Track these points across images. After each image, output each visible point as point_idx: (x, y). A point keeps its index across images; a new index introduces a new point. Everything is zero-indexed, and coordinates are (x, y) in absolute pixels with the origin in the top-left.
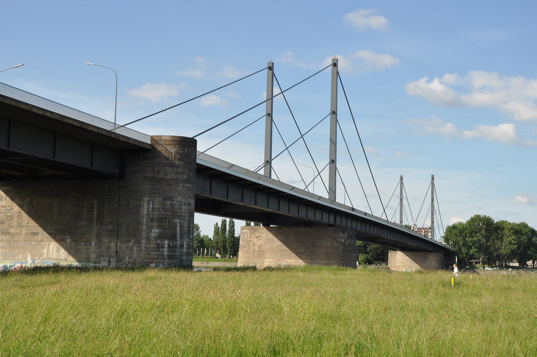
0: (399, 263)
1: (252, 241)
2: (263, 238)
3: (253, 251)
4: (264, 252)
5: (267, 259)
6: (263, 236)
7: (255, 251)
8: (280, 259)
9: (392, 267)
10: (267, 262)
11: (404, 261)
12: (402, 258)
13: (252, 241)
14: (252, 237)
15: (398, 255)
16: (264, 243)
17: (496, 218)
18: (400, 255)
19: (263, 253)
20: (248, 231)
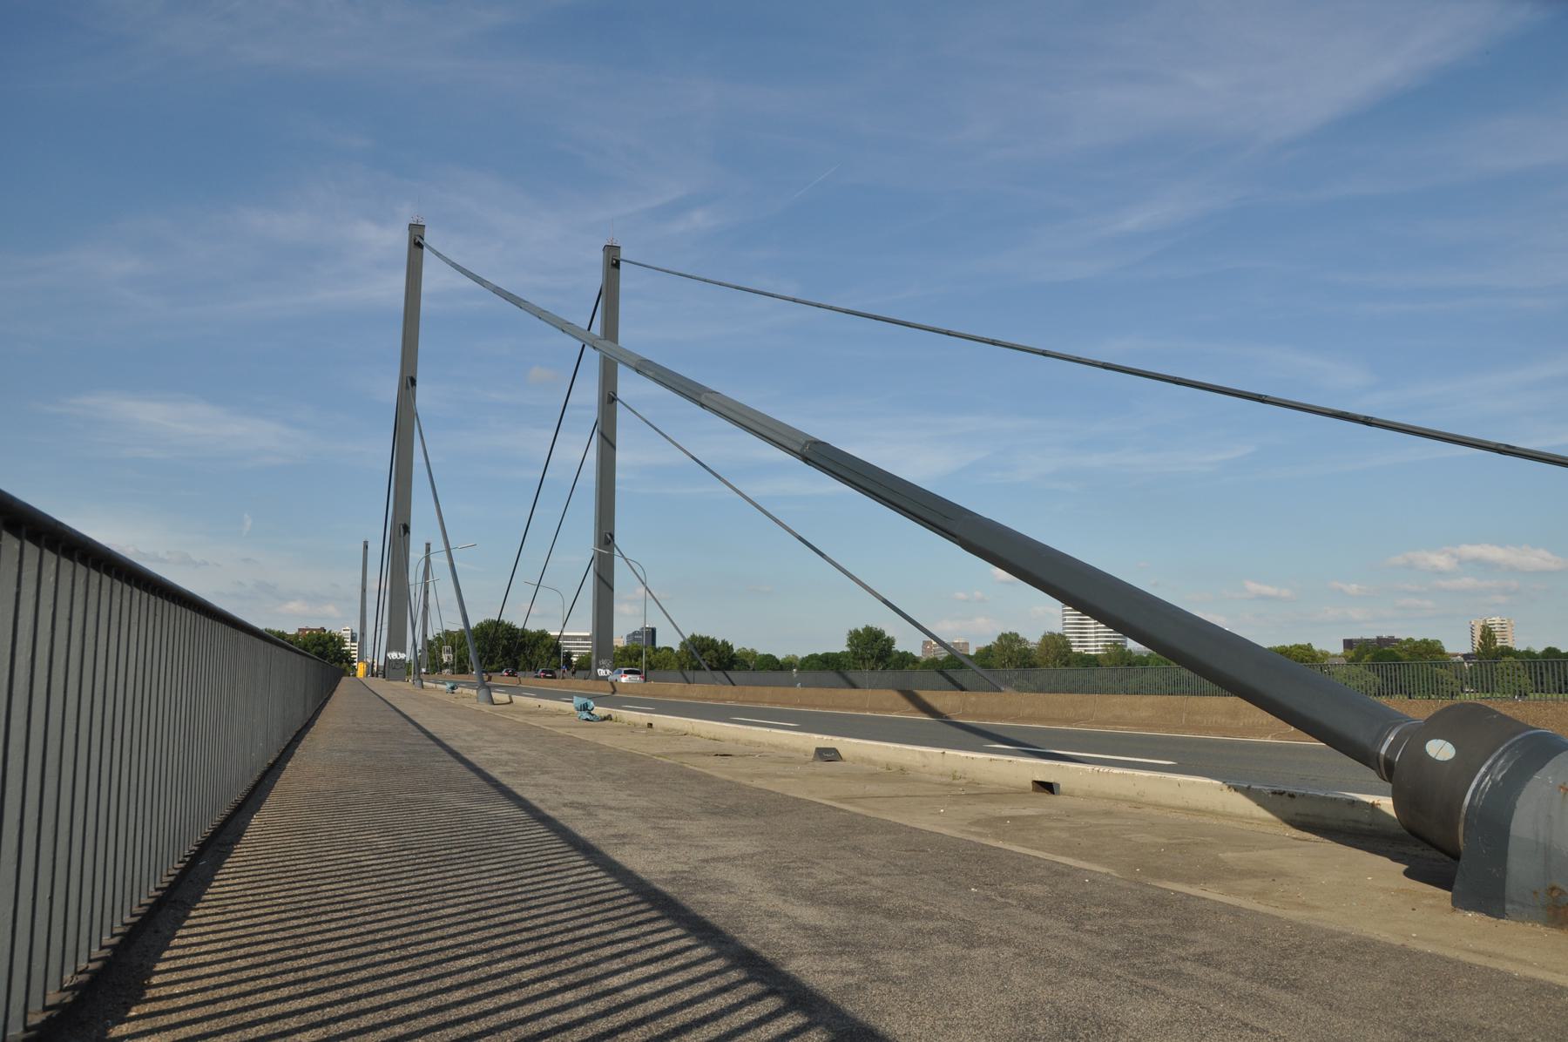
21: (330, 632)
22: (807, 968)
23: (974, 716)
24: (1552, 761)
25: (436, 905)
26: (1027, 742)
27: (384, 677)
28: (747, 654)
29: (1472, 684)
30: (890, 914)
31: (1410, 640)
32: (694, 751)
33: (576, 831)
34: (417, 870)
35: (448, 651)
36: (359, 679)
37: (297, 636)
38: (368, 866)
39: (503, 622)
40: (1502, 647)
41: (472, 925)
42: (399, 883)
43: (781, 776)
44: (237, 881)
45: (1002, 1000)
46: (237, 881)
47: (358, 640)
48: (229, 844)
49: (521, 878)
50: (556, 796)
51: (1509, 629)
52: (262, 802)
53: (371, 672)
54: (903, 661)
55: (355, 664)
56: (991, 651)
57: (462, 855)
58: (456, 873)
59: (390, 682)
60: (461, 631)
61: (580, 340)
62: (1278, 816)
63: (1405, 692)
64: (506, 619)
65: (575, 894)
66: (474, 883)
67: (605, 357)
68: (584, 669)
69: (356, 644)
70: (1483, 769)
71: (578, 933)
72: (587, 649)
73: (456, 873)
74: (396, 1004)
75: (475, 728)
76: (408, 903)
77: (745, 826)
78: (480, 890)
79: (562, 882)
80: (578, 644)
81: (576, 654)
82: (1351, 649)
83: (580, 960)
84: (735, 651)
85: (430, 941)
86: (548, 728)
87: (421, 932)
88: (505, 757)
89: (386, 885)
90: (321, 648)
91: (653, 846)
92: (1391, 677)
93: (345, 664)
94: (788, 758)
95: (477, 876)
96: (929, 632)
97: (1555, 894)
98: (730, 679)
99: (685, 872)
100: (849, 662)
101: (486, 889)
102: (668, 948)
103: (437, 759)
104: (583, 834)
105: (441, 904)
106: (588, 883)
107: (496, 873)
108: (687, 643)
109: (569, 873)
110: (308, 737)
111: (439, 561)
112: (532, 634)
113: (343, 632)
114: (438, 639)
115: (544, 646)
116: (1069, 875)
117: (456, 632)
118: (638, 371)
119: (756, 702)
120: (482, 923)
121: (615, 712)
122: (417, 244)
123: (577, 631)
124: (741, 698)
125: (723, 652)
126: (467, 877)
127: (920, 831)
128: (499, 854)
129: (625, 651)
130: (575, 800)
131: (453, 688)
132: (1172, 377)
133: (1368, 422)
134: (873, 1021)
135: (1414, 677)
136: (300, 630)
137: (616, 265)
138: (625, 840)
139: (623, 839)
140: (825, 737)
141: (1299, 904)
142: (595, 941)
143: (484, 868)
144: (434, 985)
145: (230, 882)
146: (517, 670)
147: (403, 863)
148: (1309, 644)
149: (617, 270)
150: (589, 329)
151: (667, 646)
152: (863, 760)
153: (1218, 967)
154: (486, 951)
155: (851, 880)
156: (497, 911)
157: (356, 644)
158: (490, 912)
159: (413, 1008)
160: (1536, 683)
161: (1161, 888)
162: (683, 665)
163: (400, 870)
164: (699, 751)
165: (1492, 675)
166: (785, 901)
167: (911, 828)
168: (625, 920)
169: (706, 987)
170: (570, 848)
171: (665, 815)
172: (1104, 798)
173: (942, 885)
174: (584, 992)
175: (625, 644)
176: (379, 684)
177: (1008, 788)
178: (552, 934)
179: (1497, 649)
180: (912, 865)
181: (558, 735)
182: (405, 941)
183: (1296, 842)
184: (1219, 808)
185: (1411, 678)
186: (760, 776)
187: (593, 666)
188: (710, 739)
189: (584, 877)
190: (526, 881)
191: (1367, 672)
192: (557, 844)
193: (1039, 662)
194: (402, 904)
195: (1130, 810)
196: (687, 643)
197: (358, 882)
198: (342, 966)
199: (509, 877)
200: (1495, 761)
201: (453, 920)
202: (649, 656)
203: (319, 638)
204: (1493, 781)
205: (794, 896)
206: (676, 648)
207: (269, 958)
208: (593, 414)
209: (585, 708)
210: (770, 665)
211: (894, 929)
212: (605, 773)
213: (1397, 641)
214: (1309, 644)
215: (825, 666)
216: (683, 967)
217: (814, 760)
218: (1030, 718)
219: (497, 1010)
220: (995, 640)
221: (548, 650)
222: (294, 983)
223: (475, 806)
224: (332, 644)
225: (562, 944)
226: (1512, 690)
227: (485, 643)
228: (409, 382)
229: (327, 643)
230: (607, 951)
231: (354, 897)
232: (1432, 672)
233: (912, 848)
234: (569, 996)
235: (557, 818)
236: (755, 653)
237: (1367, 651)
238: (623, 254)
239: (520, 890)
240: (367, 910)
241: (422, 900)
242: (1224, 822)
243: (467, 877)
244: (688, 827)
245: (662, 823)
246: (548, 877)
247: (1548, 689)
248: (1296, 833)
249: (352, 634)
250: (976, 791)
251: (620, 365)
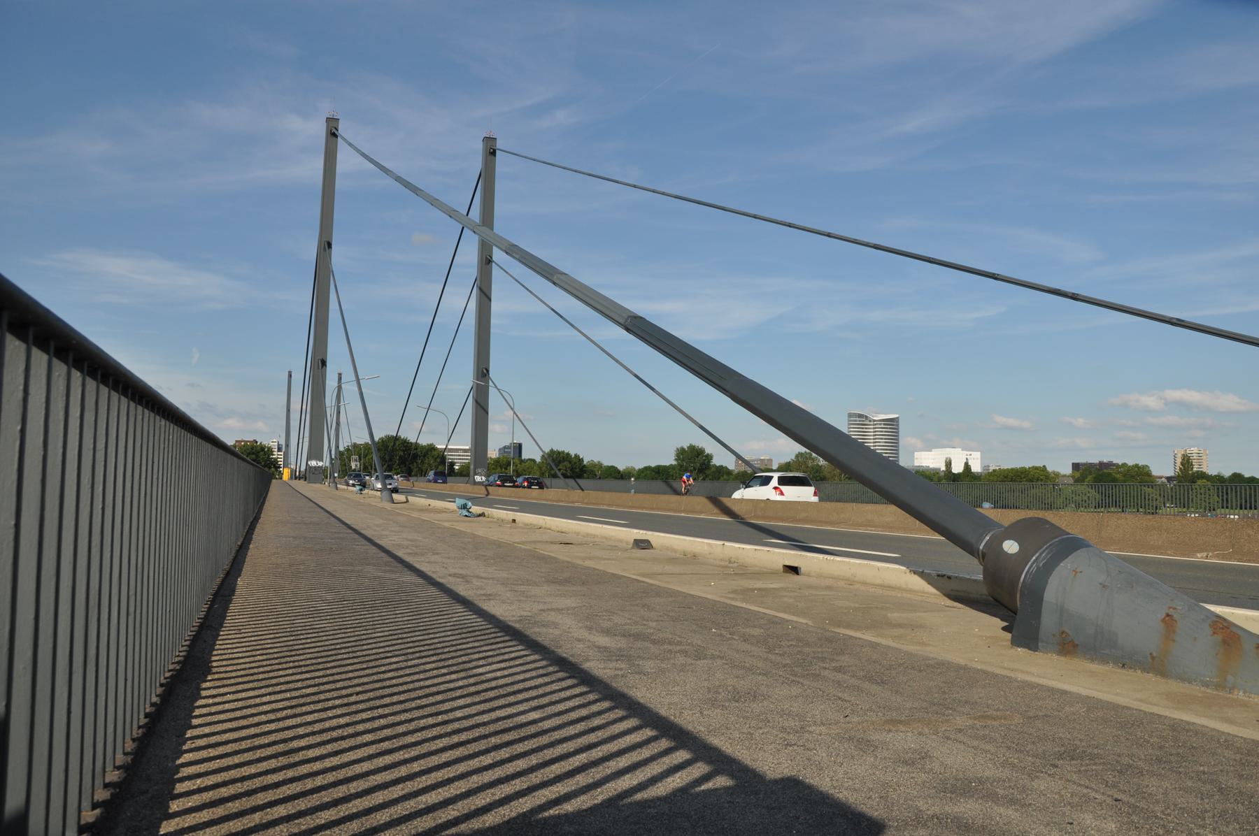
21: (261, 443)
22: (596, 667)
23: (764, 518)
24: (1073, 555)
25: (370, 631)
26: (797, 538)
27: (305, 480)
29: (1172, 501)
30: (654, 642)
31: (1124, 465)
32: (545, 540)
33: (458, 591)
34: (355, 612)
35: (356, 460)
36: (285, 481)
37: (235, 446)
38: (323, 610)
39: (400, 437)
40: (1197, 472)
41: (394, 642)
42: (344, 619)
43: (605, 559)
44: (241, 617)
45: (706, 684)
46: (241, 617)
47: (284, 450)
48: (230, 596)
49: (423, 618)
50: (443, 569)
51: (1204, 457)
52: (241, 570)
53: (294, 476)
54: (720, 473)
55: (281, 469)
56: (789, 466)
57: (383, 604)
58: (380, 614)
59: (310, 484)
60: (367, 444)
61: (461, 223)
62: (939, 591)
63: (1119, 506)
64: (402, 435)
65: (457, 627)
66: (392, 620)
67: (483, 241)
68: (464, 476)
69: (282, 453)
70: (1034, 558)
71: (459, 647)
72: (467, 459)
73: (380, 614)
74: (355, 678)
75: (381, 521)
76: (352, 630)
77: (573, 591)
78: (397, 624)
79: (449, 620)
80: (459, 455)
81: (458, 463)
82: (1078, 471)
83: (460, 660)
84: (585, 463)
85: (370, 649)
86: (436, 522)
87: (363, 645)
88: (406, 543)
89: (336, 620)
90: (254, 456)
91: (509, 601)
92: (1109, 494)
93: (273, 469)
94: (613, 546)
95: (394, 616)
97: (1064, 636)
98: (580, 486)
99: (529, 616)
100: (676, 473)
101: (401, 623)
102: (513, 655)
103: (357, 543)
104: (462, 593)
105: (373, 631)
106: (465, 622)
107: (406, 615)
108: (546, 456)
109: (453, 615)
110: (258, 527)
111: (350, 389)
112: (423, 447)
113: (271, 444)
114: (348, 450)
115: (433, 457)
116: (780, 624)
117: (361, 445)
118: (507, 253)
119: (598, 504)
120: (400, 641)
121: (488, 511)
122: (333, 134)
123: (459, 445)
124: (586, 501)
125: (575, 463)
126: (388, 617)
127: (692, 596)
128: (407, 604)
129: (497, 461)
130: (457, 572)
132: (927, 257)
133: (1074, 297)
134: (626, 690)
135: (1126, 494)
136: (237, 441)
137: (493, 153)
138: (491, 598)
139: (489, 597)
140: (642, 532)
141: (920, 643)
142: (469, 651)
143: (398, 612)
144: (375, 670)
145: (237, 617)
146: (410, 476)
147: (345, 609)
148: (1044, 466)
149: (493, 157)
150: (467, 215)
151: (530, 458)
152: (667, 548)
153: (845, 673)
154: (404, 655)
155: (636, 623)
156: (409, 635)
157: (282, 453)
158: (405, 636)
159: (365, 680)
160: (1223, 500)
161: (835, 632)
162: (543, 473)
163: (344, 612)
164: (549, 540)
165: (1188, 494)
166: (590, 633)
167: (688, 594)
168: (488, 641)
169: (534, 674)
170: (454, 601)
171: (519, 583)
172: (829, 578)
173: (694, 627)
174: (462, 674)
175: (497, 456)
176: (300, 485)
177: (765, 570)
178: (443, 647)
179: (1194, 473)
180: (679, 616)
181: (445, 528)
182: (354, 649)
183: (948, 609)
184: (904, 586)
185: (1125, 495)
186: (590, 559)
187: (472, 473)
188: (558, 532)
189: (463, 618)
190: (425, 620)
191: (1090, 490)
192: (445, 599)
193: (828, 475)
194: (349, 630)
195: (845, 586)
196: (546, 456)
197: (318, 619)
198: (320, 660)
199: (414, 617)
200: (1041, 554)
201: (382, 639)
202: (516, 466)
203: (252, 449)
204: (1038, 567)
205: (597, 631)
206: (538, 460)
207: (276, 656)
208: (473, 272)
209: (464, 507)
210: (613, 474)
211: (654, 649)
212: (479, 555)
213: (1114, 465)
214: (1044, 466)
215: (658, 476)
216: (521, 665)
217: (632, 548)
218: (804, 521)
219: (413, 682)
220: (793, 457)
221: (435, 459)
222: (294, 667)
223: (387, 575)
224: (262, 453)
225: (449, 652)
226: (1203, 507)
227: (385, 454)
228: (326, 246)
229: (259, 452)
230: (477, 656)
231: (318, 626)
232: (1141, 490)
233: (683, 606)
234: (454, 677)
235: (445, 583)
236: (601, 464)
237: (1090, 473)
238: (500, 144)
239: (422, 624)
240: (327, 633)
241: (361, 629)
242: (905, 595)
243: (388, 617)
244: (535, 591)
245: (516, 588)
246: (440, 618)
247: (1232, 506)
248: (949, 602)
249: (278, 445)
250: (742, 571)
251: (494, 248)
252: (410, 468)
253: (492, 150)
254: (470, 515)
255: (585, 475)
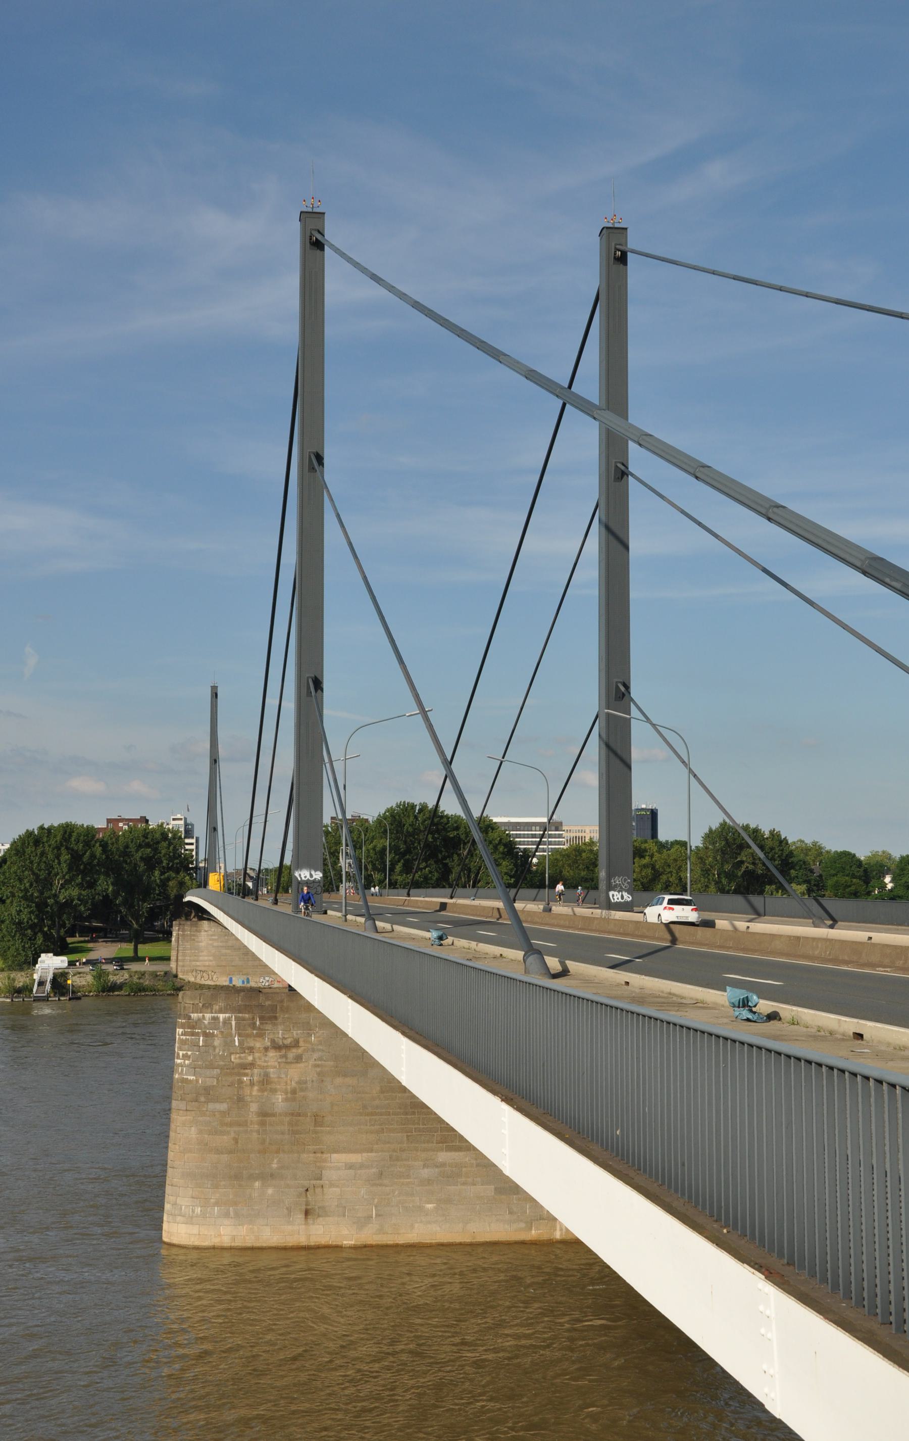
0: (206, 958)
1: (252, 1065)
2: (313, 1050)
3: (265, 1114)
4: (318, 1120)
5: (335, 1156)
6: (310, 1042)
7: (274, 1115)
8: (402, 1150)
9: (183, 972)
10: (339, 1169)
11: (224, 951)
12: (216, 944)
13: (252, 1065)
14: (251, 1050)
15: (203, 933)
16: (319, 1074)
17: (862, 854)
18: (210, 933)
19: (316, 1123)
20: (229, 1019)
28: (807, 850)
96: (660, 494)
118: (526, 378)
121: (786, 1010)
124: (900, 963)
125: (772, 849)
131: (441, 938)
136: (109, 821)
137: (622, 259)
149: (625, 267)
157: (193, 841)
187: (602, 885)
203: (145, 836)
209: (745, 1003)
224: (165, 844)
229: (158, 843)
236: (820, 848)
238: (633, 242)
249: (186, 825)
252: (446, 864)
253: (619, 253)
254: (755, 1017)
255: (792, 871)
